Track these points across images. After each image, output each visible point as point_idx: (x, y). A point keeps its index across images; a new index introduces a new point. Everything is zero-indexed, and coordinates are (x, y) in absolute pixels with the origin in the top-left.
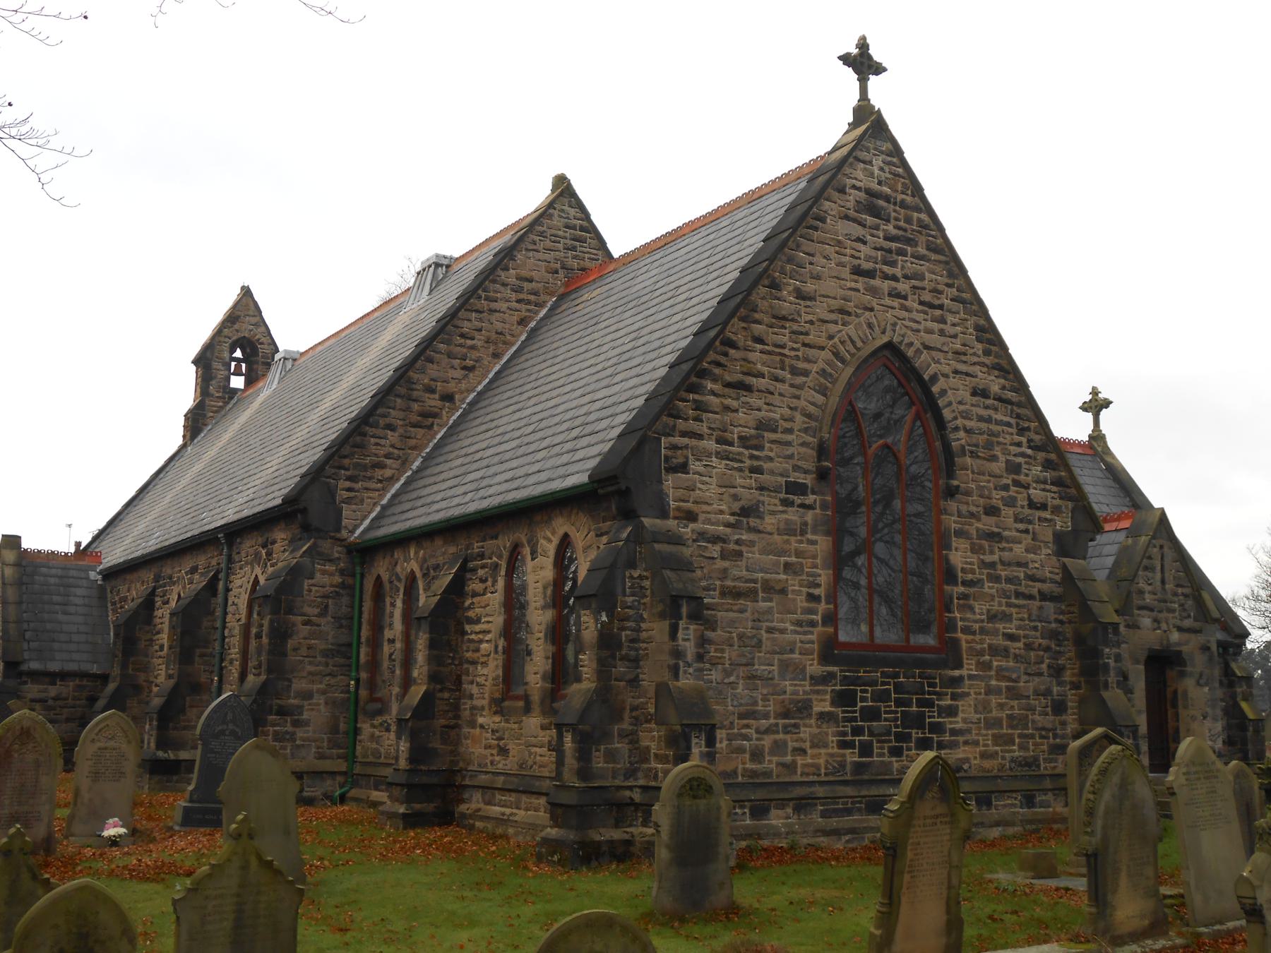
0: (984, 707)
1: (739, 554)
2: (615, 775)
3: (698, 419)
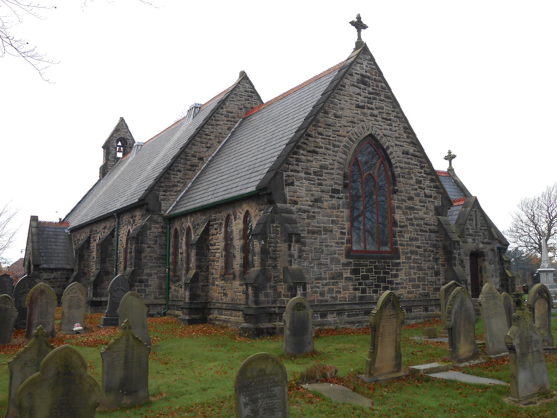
3: (297, 165)
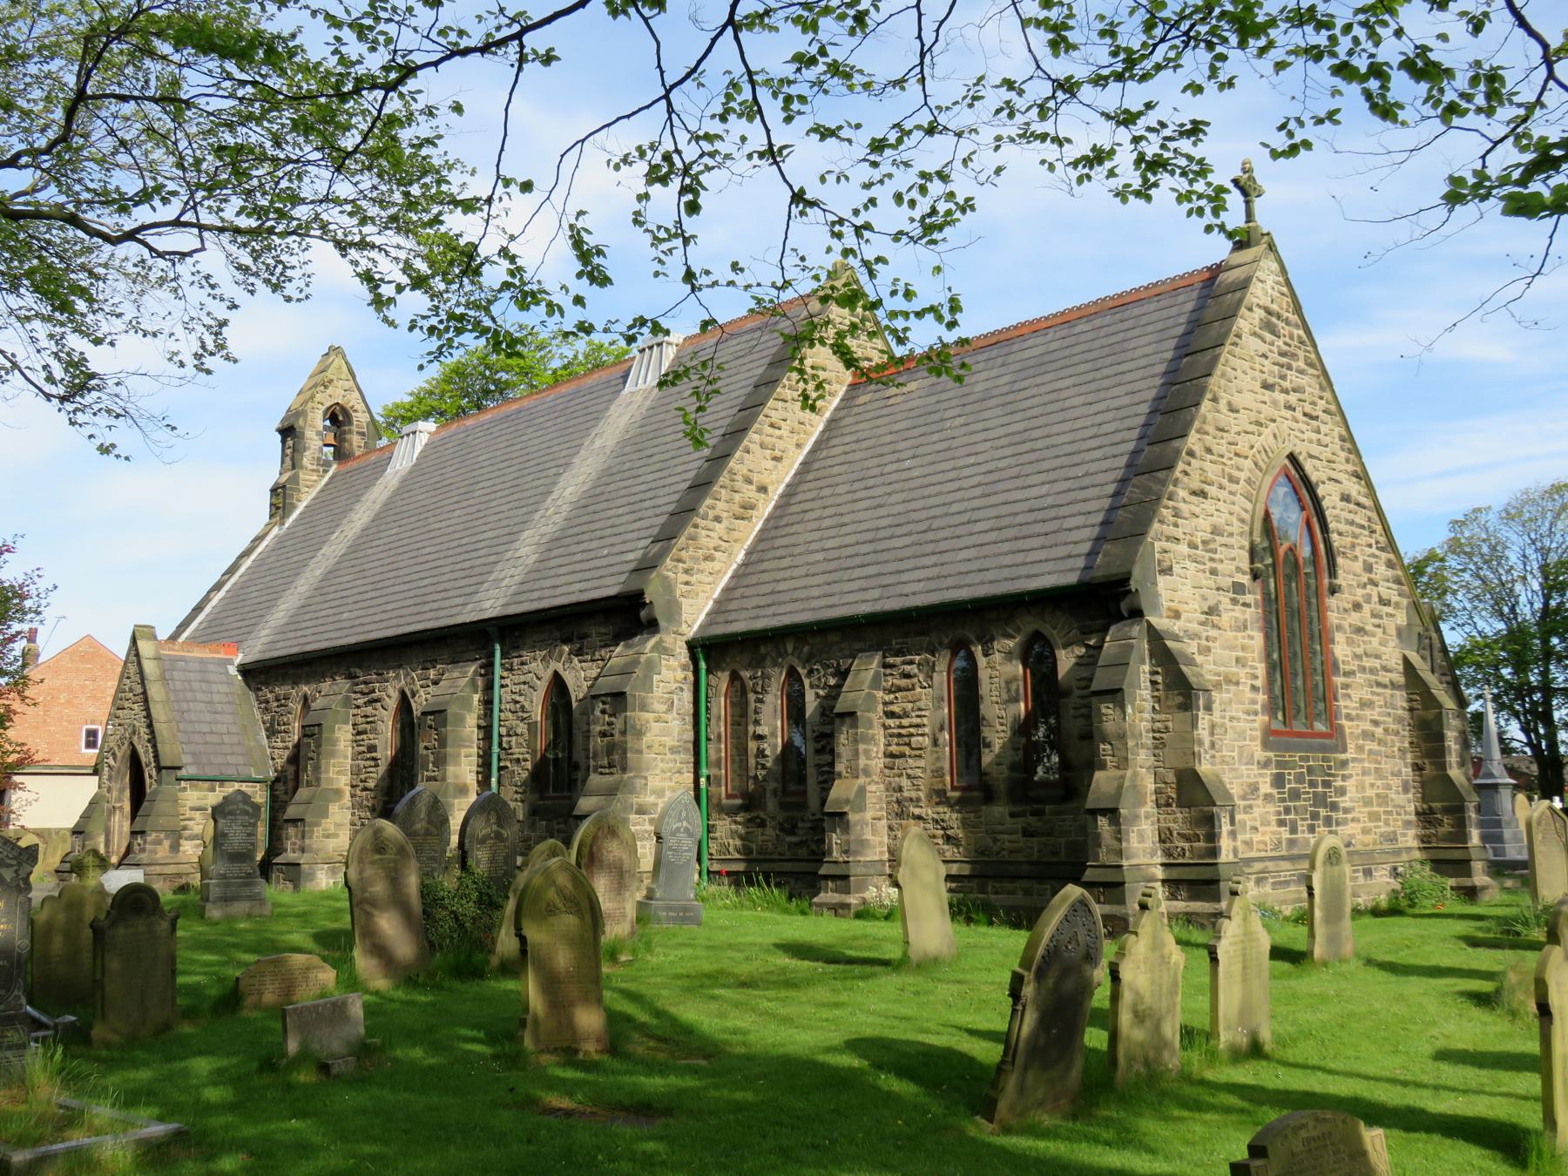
0: (1361, 787)
3: (1176, 525)
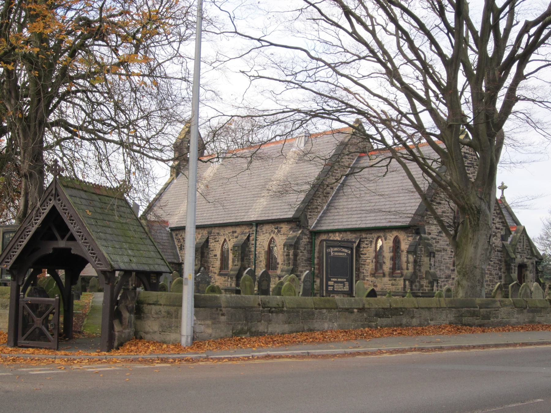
1: (438, 242)
2: (416, 290)
